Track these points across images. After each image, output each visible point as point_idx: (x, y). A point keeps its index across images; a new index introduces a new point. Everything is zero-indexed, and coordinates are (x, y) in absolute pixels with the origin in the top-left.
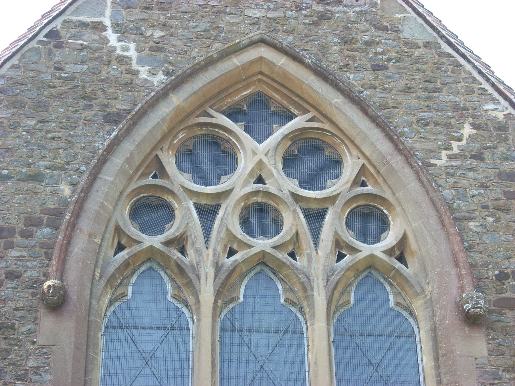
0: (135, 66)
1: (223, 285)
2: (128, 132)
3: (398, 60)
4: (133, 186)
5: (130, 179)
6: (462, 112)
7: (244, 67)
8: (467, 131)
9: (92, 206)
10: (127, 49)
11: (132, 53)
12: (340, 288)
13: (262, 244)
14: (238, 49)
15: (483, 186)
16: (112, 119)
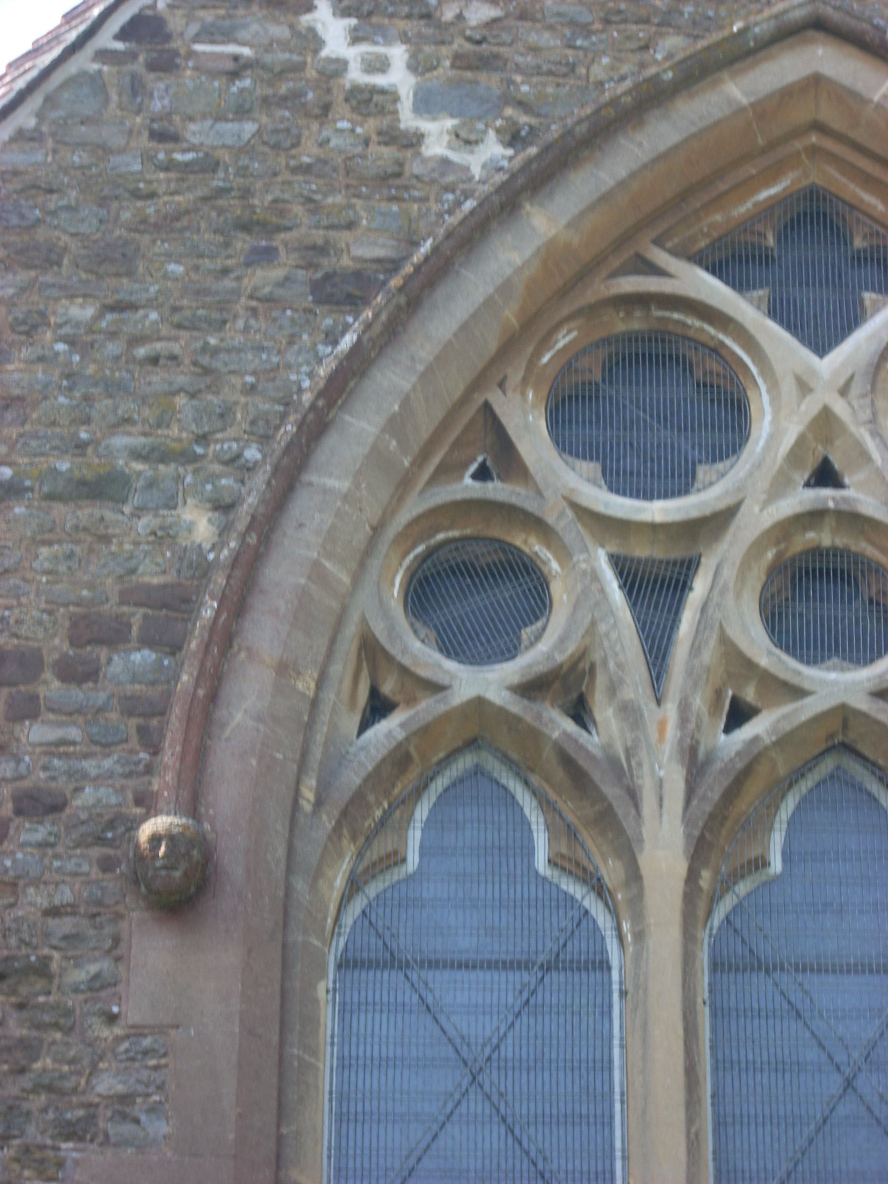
0: (408, 119)
5: (405, 484)
7: (764, 109)
9: (284, 573)
10: (380, 65)
11: (399, 78)
14: (740, 54)
16: (341, 291)
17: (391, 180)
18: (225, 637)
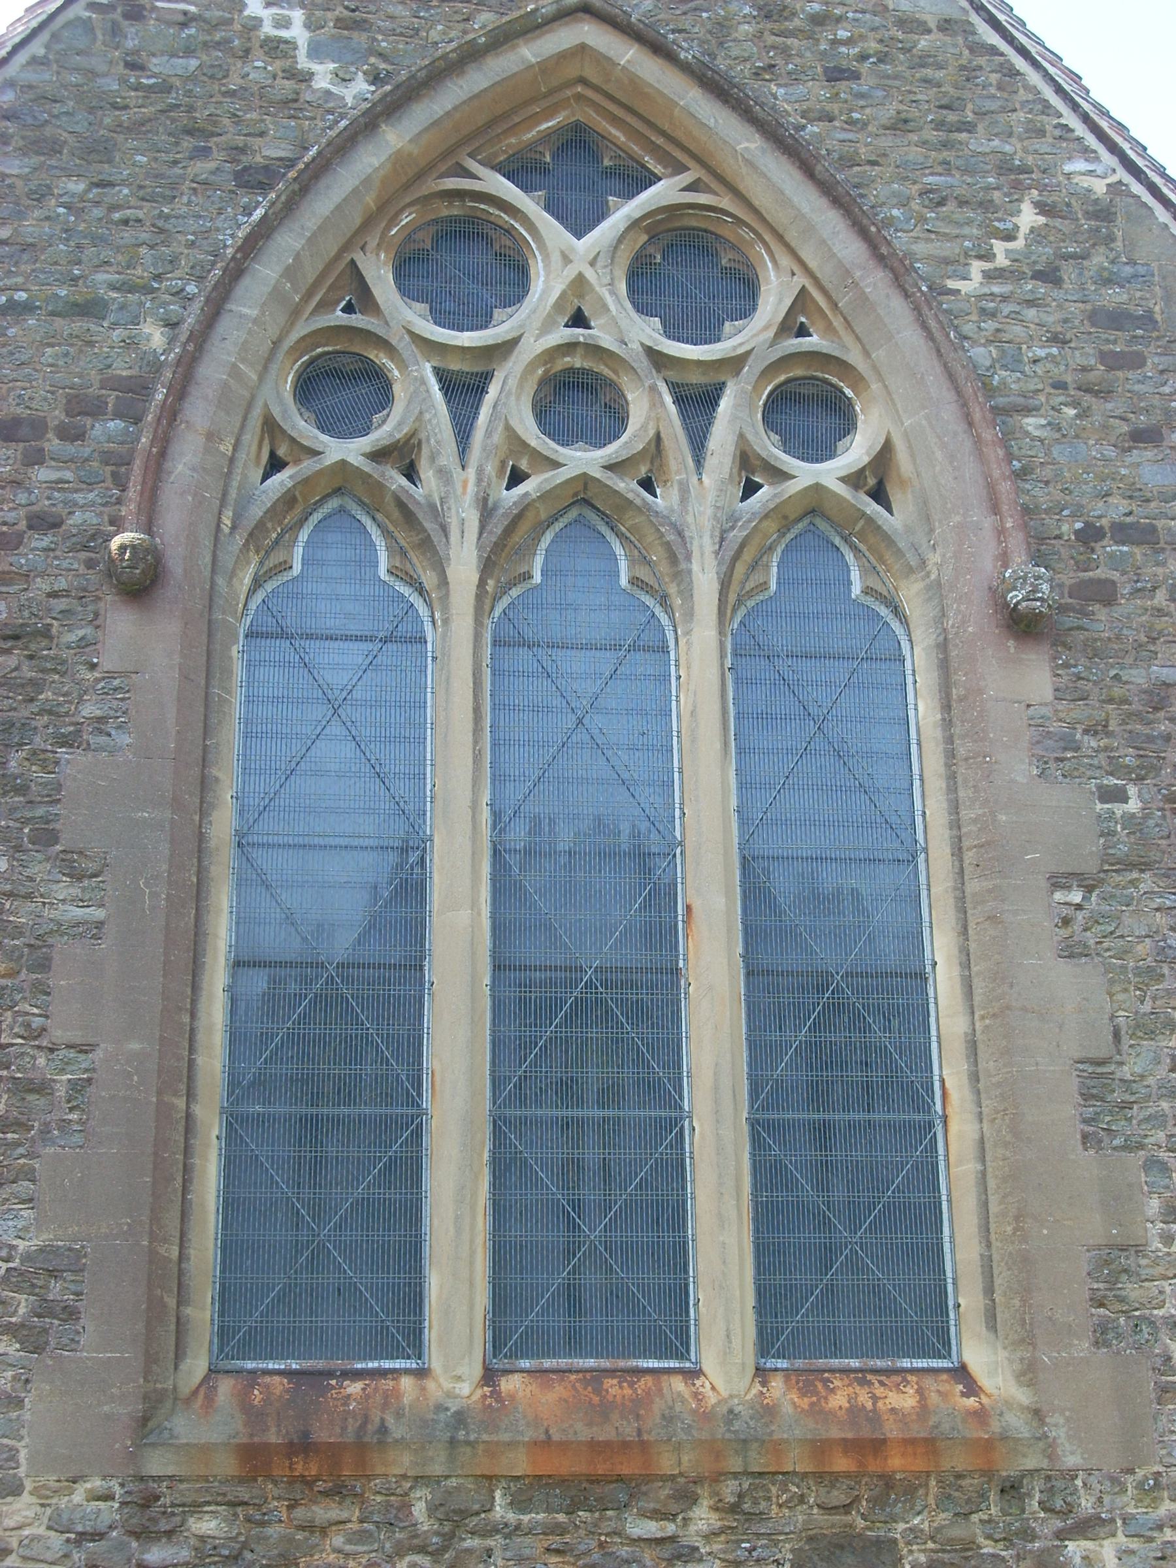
1: (499, 546)
2: (289, 208)
3: (882, 58)
4: (301, 330)
5: (295, 313)
6: (1015, 175)
7: (547, 67)
8: (1028, 218)
10: (284, 23)
11: (298, 32)
12: (748, 556)
13: (583, 460)
15: (1056, 339)
16: (255, 179)
17: (291, 103)
18: (171, 414)
